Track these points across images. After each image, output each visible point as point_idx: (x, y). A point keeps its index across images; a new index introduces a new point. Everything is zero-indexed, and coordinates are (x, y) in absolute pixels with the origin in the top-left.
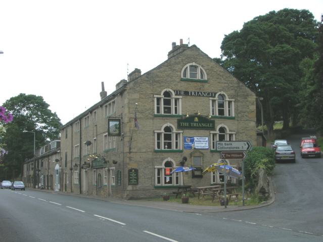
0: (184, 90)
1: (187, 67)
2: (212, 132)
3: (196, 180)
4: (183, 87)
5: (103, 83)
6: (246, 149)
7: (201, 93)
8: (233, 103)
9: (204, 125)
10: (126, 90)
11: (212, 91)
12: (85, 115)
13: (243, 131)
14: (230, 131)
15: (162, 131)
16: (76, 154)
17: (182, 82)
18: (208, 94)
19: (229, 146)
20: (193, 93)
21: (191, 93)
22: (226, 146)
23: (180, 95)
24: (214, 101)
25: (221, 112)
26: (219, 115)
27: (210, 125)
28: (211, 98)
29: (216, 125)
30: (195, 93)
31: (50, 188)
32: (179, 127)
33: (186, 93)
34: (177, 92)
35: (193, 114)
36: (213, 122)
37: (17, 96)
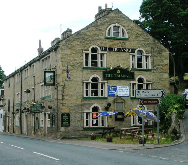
4: (108, 44)
5: (40, 41)
7: (123, 49)
11: (133, 48)
13: (158, 81)
14: (147, 81)
20: (116, 50)
21: (114, 49)
22: (144, 94)
23: (105, 50)
24: (133, 56)
25: (140, 65)
28: (131, 54)
29: (135, 76)
30: (118, 49)
32: (104, 78)
33: (110, 49)
34: (102, 48)
35: (115, 66)
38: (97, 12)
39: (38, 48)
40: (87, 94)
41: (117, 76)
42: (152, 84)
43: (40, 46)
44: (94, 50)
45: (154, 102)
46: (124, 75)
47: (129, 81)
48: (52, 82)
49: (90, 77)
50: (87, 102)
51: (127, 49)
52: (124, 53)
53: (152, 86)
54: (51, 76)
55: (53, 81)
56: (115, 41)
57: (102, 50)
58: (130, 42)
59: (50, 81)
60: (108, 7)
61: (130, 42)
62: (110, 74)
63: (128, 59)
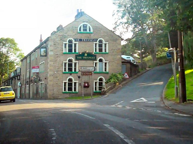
1: (81, 26)
2: (94, 62)
3: (86, 89)
4: (79, 37)
5: (41, 35)
6: (93, 71)
7: (89, 39)
8: (107, 44)
10: (49, 40)
11: (95, 38)
12: (32, 53)
14: (105, 61)
15: (67, 62)
16: (28, 76)
17: (78, 34)
18: (93, 40)
19: (85, 69)
20: (84, 40)
21: (83, 40)
22: (84, 69)
23: (77, 41)
25: (101, 50)
26: (99, 52)
28: (94, 42)
29: (97, 58)
30: (86, 40)
32: (76, 59)
33: (81, 40)
34: (76, 40)
35: (83, 51)
36: (95, 56)
37: (77, 14)
38: (76, 14)
39: (40, 40)
40: (65, 70)
41: (85, 58)
43: (41, 38)
44: (70, 41)
45: (90, 74)
47: (93, 61)
48: (45, 54)
49: (67, 59)
50: (64, 75)
53: (109, 64)
54: (44, 50)
55: (45, 54)
56: (85, 35)
57: (75, 41)
59: (44, 54)
60: (82, 11)
62: (80, 56)
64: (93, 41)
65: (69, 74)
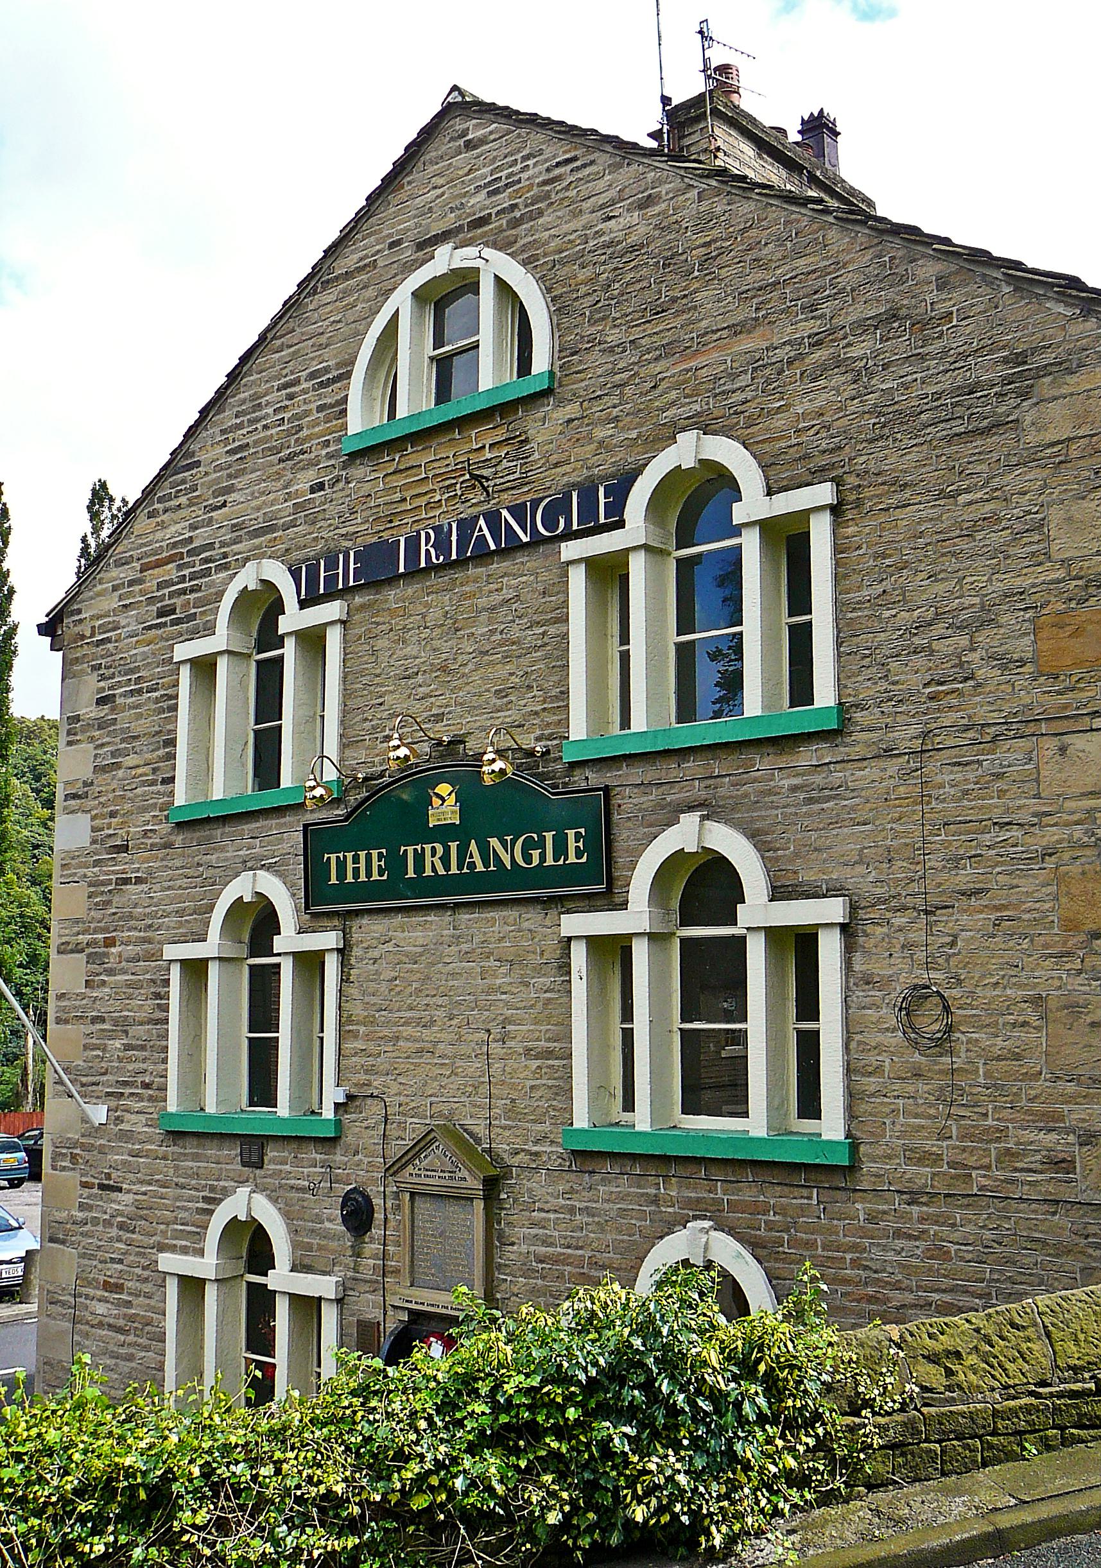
0: (364, 530)
2: (575, 924)
7: (493, 519)
9: (508, 853)
13: (965, 877)
14: (779, 893)
21: (413, 544)
24: (609, 574)
27: (560, 848)
28: (570, 550)
29: (624, 835)
30: (442, 545)
31: (92, 889)
32: (320, 898)
33: (379, 569)
42: (835, 510)
46: (494, 842)
51: (536, 503)
52: (505, 565)
58: (572, 410)
61: (572, 410)
63: (552, 630)
64: (550, 524)
65: (275, 952)
